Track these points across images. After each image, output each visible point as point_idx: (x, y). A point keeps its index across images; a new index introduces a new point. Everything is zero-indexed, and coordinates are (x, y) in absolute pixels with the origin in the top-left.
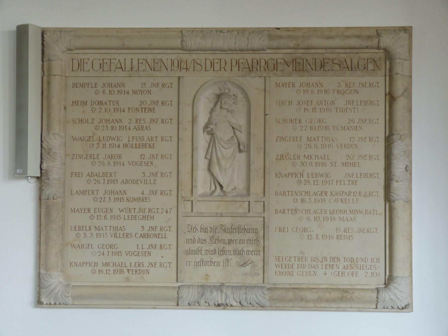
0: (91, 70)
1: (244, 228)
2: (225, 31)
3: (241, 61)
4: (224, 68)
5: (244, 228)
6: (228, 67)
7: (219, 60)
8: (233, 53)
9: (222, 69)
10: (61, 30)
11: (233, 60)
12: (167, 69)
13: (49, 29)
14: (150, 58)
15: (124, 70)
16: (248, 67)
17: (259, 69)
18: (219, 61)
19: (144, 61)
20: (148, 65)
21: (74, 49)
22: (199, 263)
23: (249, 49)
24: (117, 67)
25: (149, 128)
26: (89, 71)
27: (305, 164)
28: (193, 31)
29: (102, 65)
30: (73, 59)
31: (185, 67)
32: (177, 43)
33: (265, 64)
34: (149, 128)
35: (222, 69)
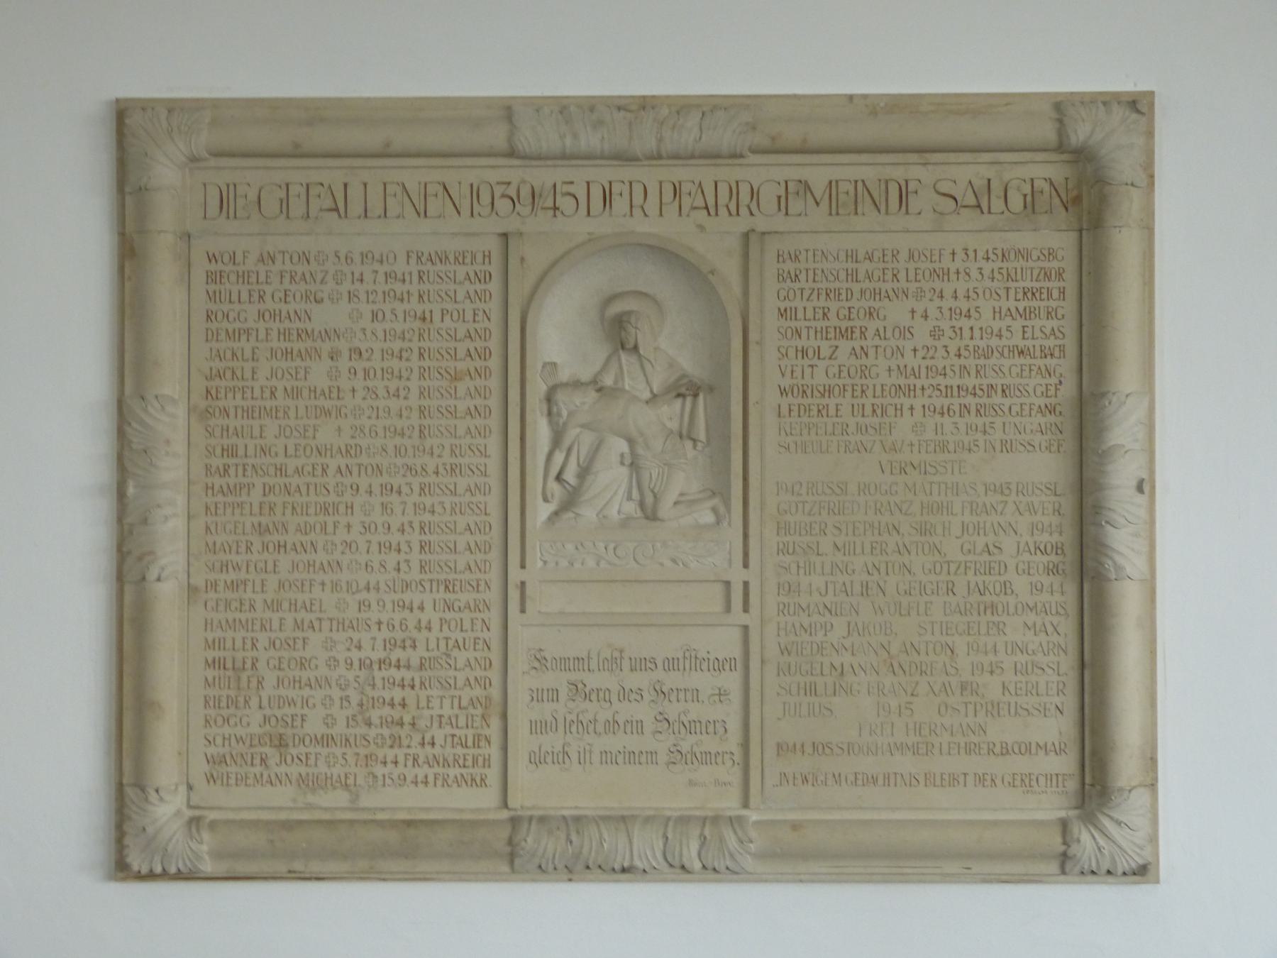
0: (1006, 212)
1: (609, 658)
2: (634, 107)
3: (685, 188)
4: (727, 206)
5: (609, 658)
6: (652, 205)
7: (853, 183)
8: (442, 167)
9: (637, 212)
10: (173, 107)
11: (789, 183)
12: (459, 213)
13: (146, 105)
14: (413, 180)
15: (343, 215)
16: (704, 205)
17: (734, 211)
18: (303, 190)
19: (399, 190)
20: (871, 201)
21: (207, 156)
22: (629, 727)
23: (664, 154)
24: (695, 205)
25: (1060, 331)
26: (920, 213)
27: (373, 526)
28: (537, 105)
29: (783, 200)
30: (205, 185)
31: (551, 205)
32: (496, 136)
33: (731, 198)
34: (1060, 331)
35: (637, 212)
